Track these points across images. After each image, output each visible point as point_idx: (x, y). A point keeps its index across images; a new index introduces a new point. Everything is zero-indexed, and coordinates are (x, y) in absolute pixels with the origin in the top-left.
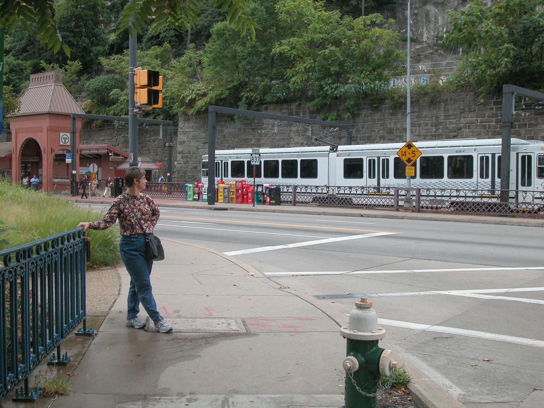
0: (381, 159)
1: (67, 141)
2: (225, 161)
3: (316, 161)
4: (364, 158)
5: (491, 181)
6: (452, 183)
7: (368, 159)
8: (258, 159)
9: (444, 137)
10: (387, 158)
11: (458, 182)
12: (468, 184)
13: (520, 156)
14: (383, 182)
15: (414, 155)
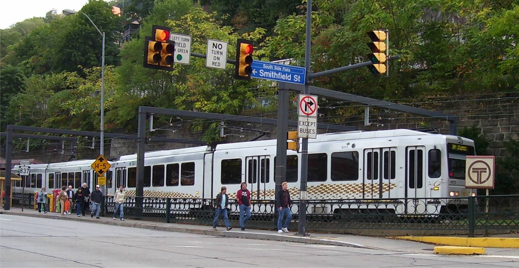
1: (484, 176)
6: (335, 186)
8: (27, 171)
10: (267, 157)
12: (353, 187)
15: (104, 167)
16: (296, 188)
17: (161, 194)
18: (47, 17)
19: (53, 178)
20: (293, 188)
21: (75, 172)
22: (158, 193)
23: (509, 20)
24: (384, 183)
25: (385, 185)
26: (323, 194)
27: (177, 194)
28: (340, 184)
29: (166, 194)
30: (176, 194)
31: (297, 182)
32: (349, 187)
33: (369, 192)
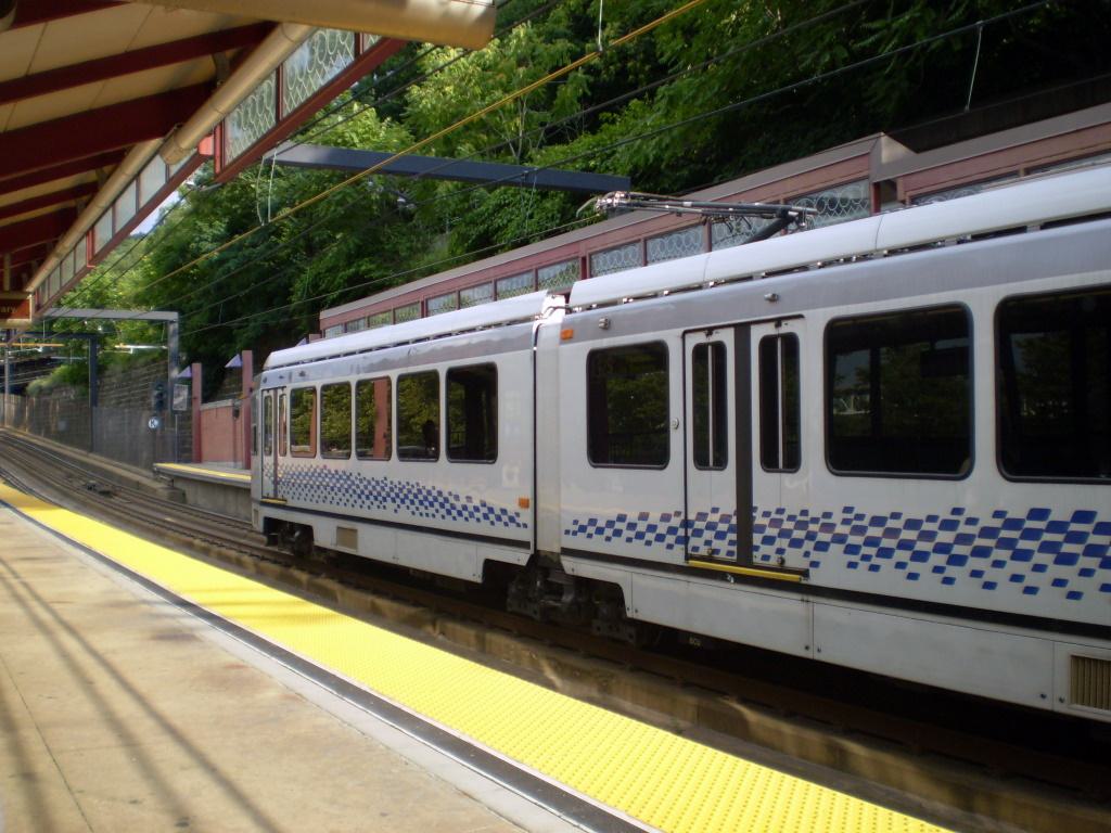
0: (757, 334)
2: (770, 330)
3: (490, 370)
9: (34, 262)
10: (785, 328)
14: (770, 489)
16: (967, 514)
17: (383, 489)
20: (945, 515)
21: (318, 385)
22: (373, 483)
23: (459, 154)
27: (435, 493)
29: (396, 491)
30: (429, 493)
31: (726, 470)
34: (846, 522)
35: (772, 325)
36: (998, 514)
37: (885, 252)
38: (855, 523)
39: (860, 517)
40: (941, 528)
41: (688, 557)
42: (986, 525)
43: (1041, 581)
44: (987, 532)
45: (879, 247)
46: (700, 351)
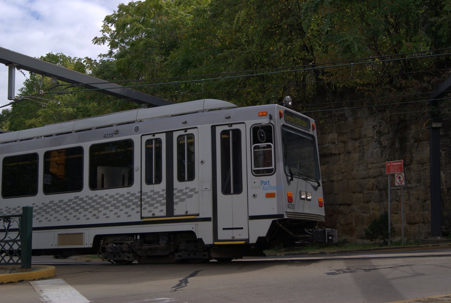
0: (176, 135)
4: (136, 138)
5: (165, 188)
7: (145, 139)
10: (189, 132)
11: (186, 188)
13: (219, 130)
16: (36, 205)
18: (64, 55)
19: (254, 152)
24: (176, 189)
25: (178, 192)
26: (68, 213)
28: (104, 195)
32: (120, 199)
33: (41, 209)
34: (6, 211)
35: (183, 131)
36: (43, 203)
37: (139, 121)
38: (8, 210)
39: (10, 209)
40: (12, 210)
41: (142, 218)
42: (41, 206)
43: (89, 215)
44: (41, 208)
45: (74, 130)
46: (149, 142)
